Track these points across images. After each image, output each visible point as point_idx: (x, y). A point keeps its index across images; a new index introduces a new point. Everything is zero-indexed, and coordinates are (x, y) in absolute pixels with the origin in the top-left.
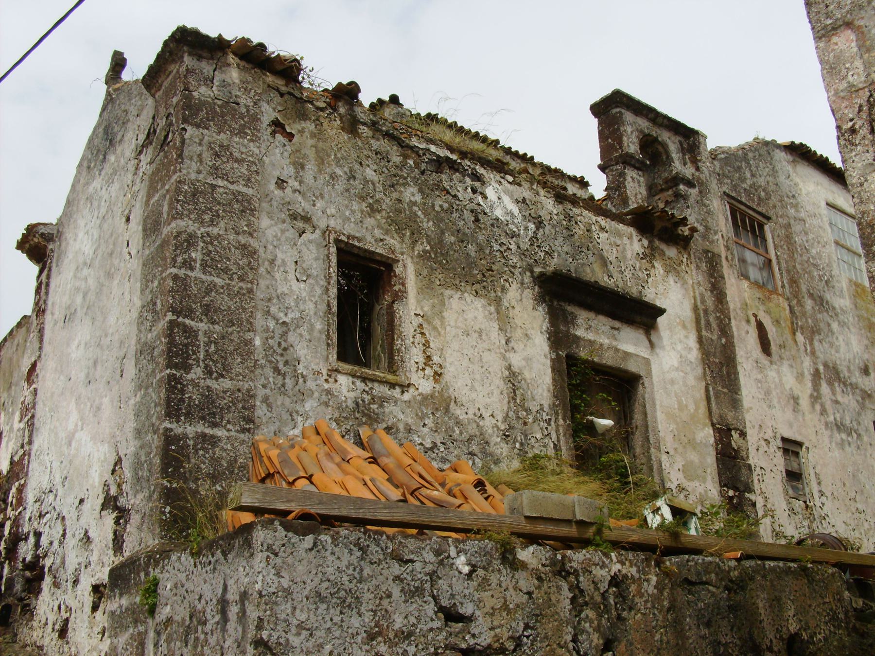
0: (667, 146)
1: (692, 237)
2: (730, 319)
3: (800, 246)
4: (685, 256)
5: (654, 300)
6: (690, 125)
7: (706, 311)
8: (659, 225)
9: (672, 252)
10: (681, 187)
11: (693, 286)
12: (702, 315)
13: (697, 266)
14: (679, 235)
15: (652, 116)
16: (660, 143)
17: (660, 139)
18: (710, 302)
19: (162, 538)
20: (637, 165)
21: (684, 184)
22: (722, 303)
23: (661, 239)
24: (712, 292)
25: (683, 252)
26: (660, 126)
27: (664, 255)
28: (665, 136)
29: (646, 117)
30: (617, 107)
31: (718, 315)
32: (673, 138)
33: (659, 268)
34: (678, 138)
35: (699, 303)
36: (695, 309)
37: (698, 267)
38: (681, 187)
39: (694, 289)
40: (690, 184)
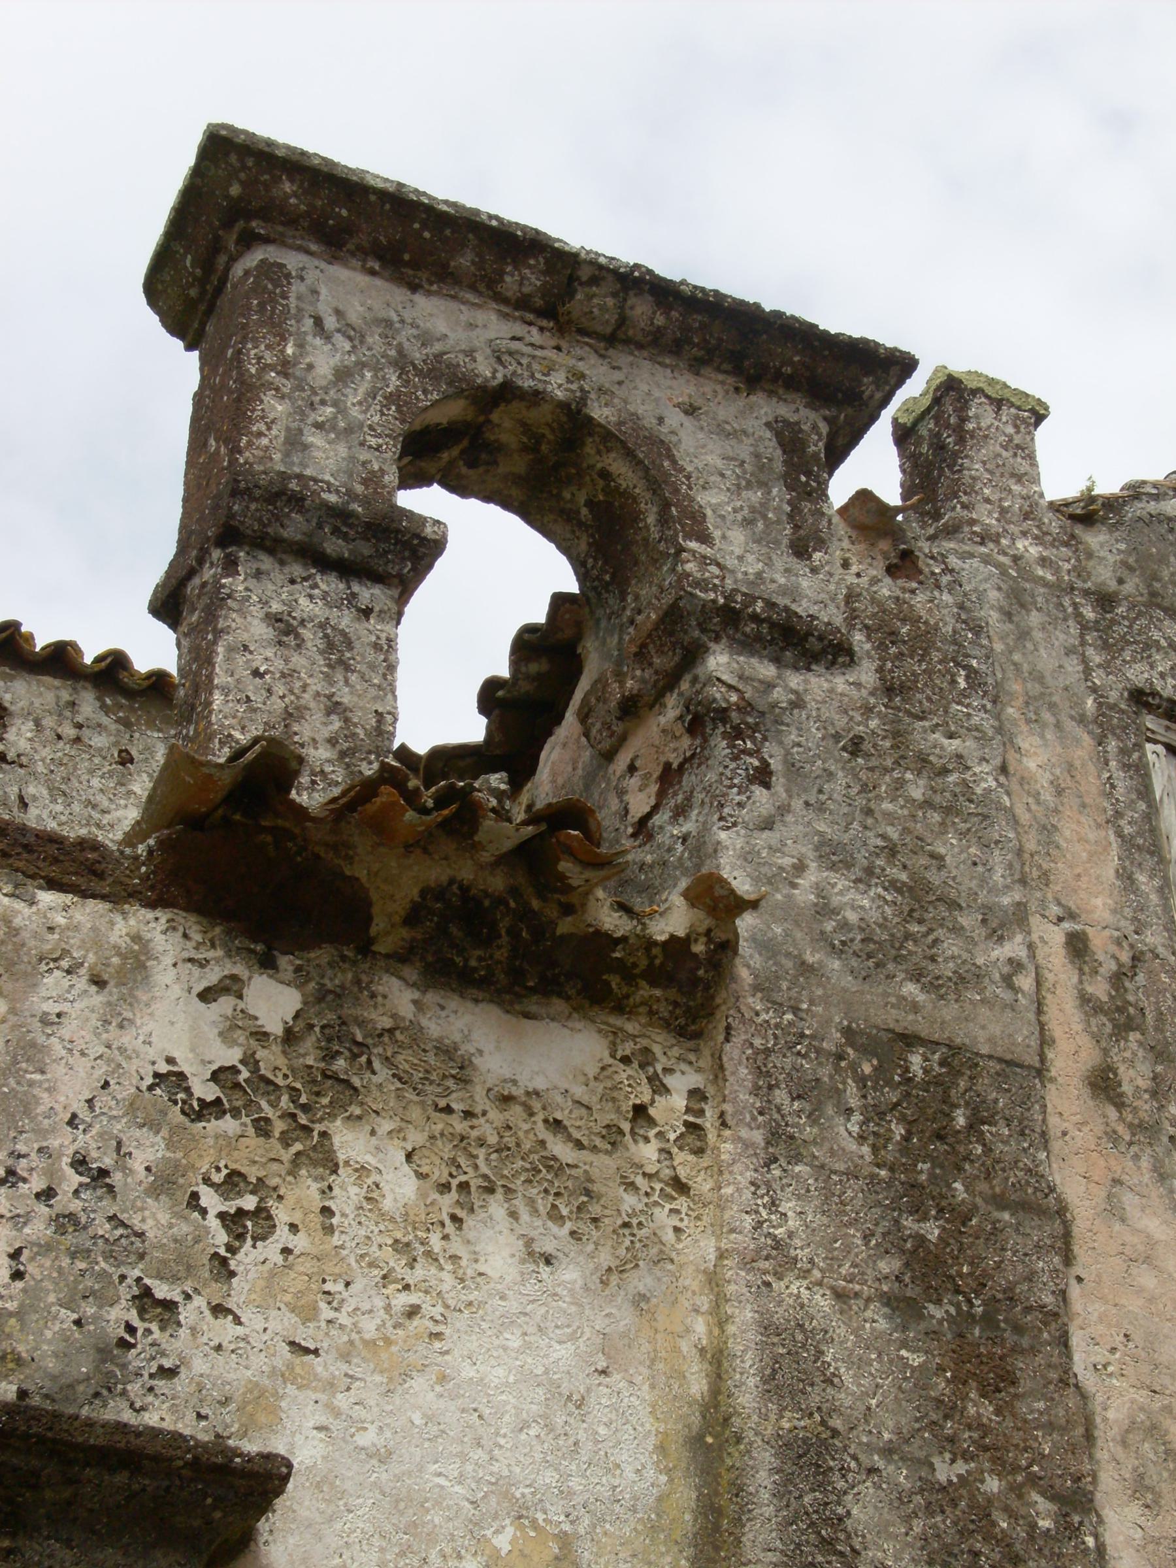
0: (665, 449)
1: (726, 947)
2: (1077, 1501)
3: (282, 234)
4: (681, 1083)
5: (260, 1402)
6: (837, 318)
7: (812, 1458)
8: (394, 882)
9: (554, 1058)
10: (719, 662)
11: (713, 1280)
12: (762, 1480)
13: (775, 1135)
14: (604, 940)
15: (527, 279)
16: (608, 438)
17: (599, 412)
18: (871, 1373)
19: (323, 1457)
20: (334, 546)
21: (748, 645)
22: (999, 1382)
23: (447, 973)
24: (903, 1307)
25: (660, 1044)
26: (614, 338)
27: (462, 1071)
28: (647, 396)
29: (486, 286)
30: (249, 240)
31: (945, 1471)
32: (727, 407)
33: (380, 1161)
34: (765, 409)
35: (747, 1395)
36: (709, 1442)
37: (781, 1144)
38: (719, 662)
39: (720, 1300)
40: (796, 641)
